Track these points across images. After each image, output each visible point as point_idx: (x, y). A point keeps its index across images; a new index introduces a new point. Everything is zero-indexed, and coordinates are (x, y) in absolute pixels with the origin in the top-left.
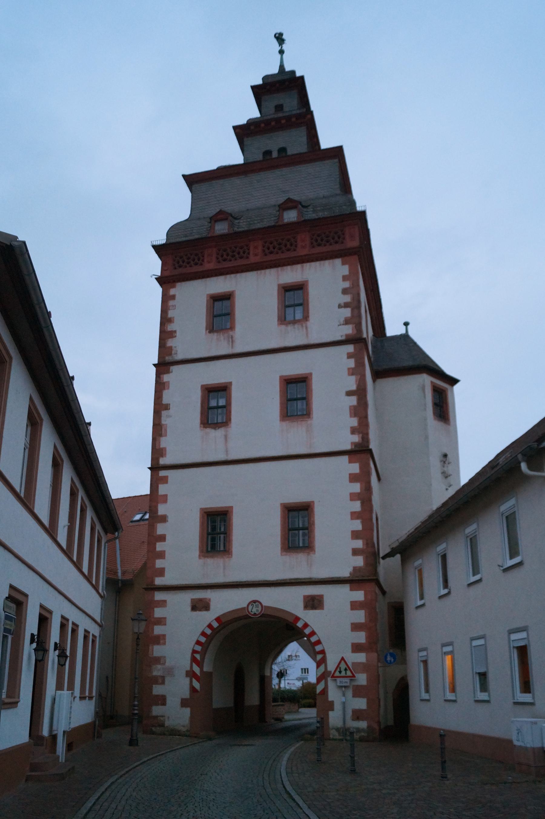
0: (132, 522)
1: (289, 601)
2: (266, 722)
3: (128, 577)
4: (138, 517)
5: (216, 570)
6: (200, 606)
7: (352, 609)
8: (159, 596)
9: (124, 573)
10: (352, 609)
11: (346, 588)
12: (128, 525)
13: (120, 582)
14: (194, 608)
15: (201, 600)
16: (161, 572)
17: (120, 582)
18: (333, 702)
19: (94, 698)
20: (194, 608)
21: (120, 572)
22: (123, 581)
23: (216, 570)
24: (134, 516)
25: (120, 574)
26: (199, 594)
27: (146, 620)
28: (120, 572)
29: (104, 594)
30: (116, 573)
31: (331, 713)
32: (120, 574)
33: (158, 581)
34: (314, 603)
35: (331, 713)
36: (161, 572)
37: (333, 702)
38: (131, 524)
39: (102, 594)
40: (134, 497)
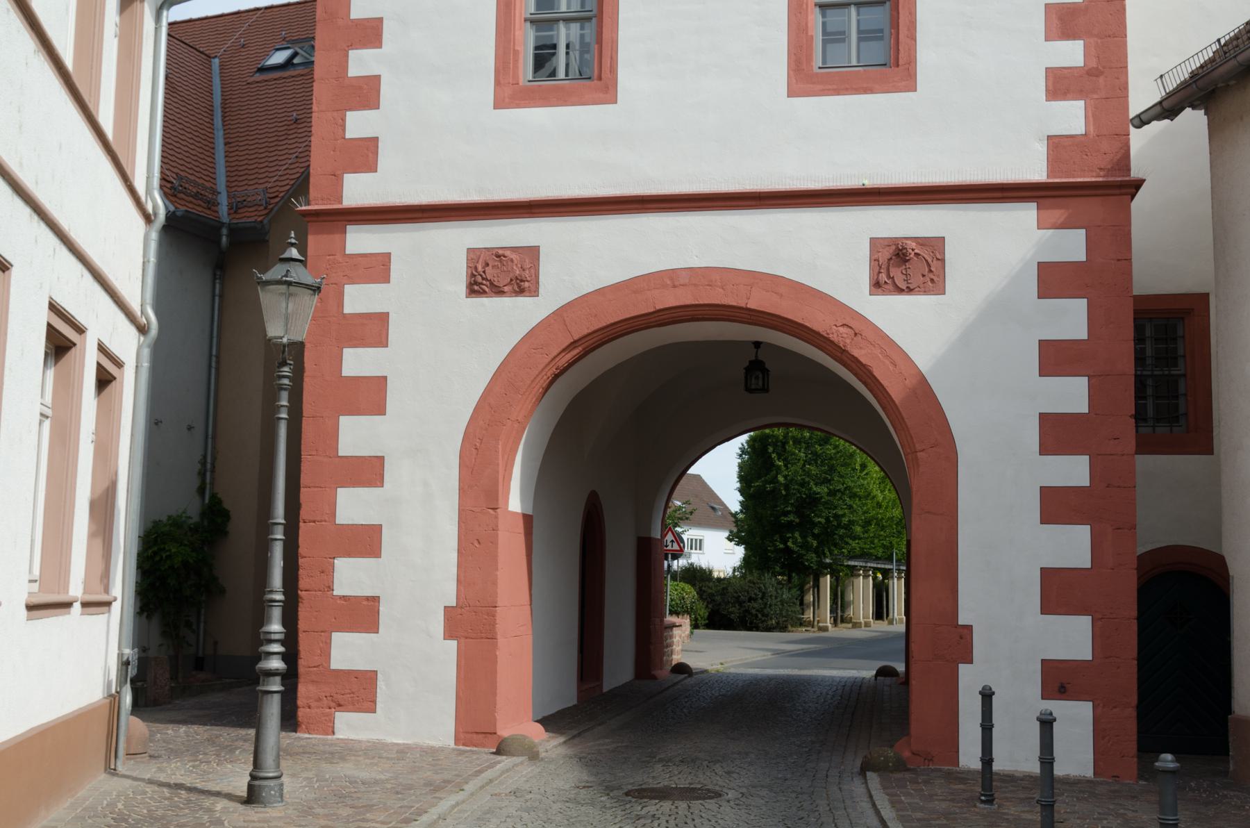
0: (262, 70)
1: (823, 260)
2: (654, 678)
3: (249, 217)
4: (279, 57)
5: (557, 146)
6: (495, 276)
7: (376, 530)
8: (360, 240)
9: (234, 208)
10: (376, 530)
11: (1026, 214)
12: (251, 80)
13: (224, 231)
14: (478, 285)
15: (499, 255)
16: (365, 155)
17: (224, 231)
18: (969, 628)
19: (116, 607)
20: (478, 285)
21: (223, 200)
22: (234, 231)
23: (557, 146)
24: (268, 56)
25: (223, 210)
26: (498, 238)
27: (316, 289)
28: (223, 200)
29: (155, 207)
30: (212, 204)
31: (963, 669)
32: (223, 210)
33: (358, 190)
34: (905, 267)
35: (963, 669)
36: (365, 155)
37: (969, 628)
38: (258, 77)
39: (150, 208)
40: (266, 8)
